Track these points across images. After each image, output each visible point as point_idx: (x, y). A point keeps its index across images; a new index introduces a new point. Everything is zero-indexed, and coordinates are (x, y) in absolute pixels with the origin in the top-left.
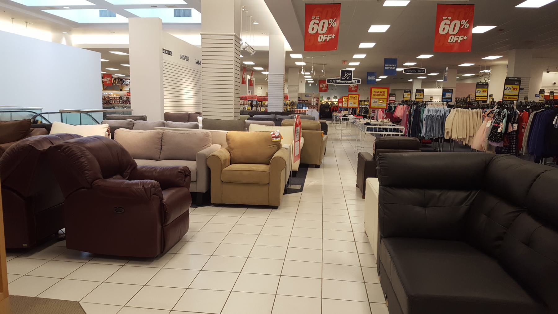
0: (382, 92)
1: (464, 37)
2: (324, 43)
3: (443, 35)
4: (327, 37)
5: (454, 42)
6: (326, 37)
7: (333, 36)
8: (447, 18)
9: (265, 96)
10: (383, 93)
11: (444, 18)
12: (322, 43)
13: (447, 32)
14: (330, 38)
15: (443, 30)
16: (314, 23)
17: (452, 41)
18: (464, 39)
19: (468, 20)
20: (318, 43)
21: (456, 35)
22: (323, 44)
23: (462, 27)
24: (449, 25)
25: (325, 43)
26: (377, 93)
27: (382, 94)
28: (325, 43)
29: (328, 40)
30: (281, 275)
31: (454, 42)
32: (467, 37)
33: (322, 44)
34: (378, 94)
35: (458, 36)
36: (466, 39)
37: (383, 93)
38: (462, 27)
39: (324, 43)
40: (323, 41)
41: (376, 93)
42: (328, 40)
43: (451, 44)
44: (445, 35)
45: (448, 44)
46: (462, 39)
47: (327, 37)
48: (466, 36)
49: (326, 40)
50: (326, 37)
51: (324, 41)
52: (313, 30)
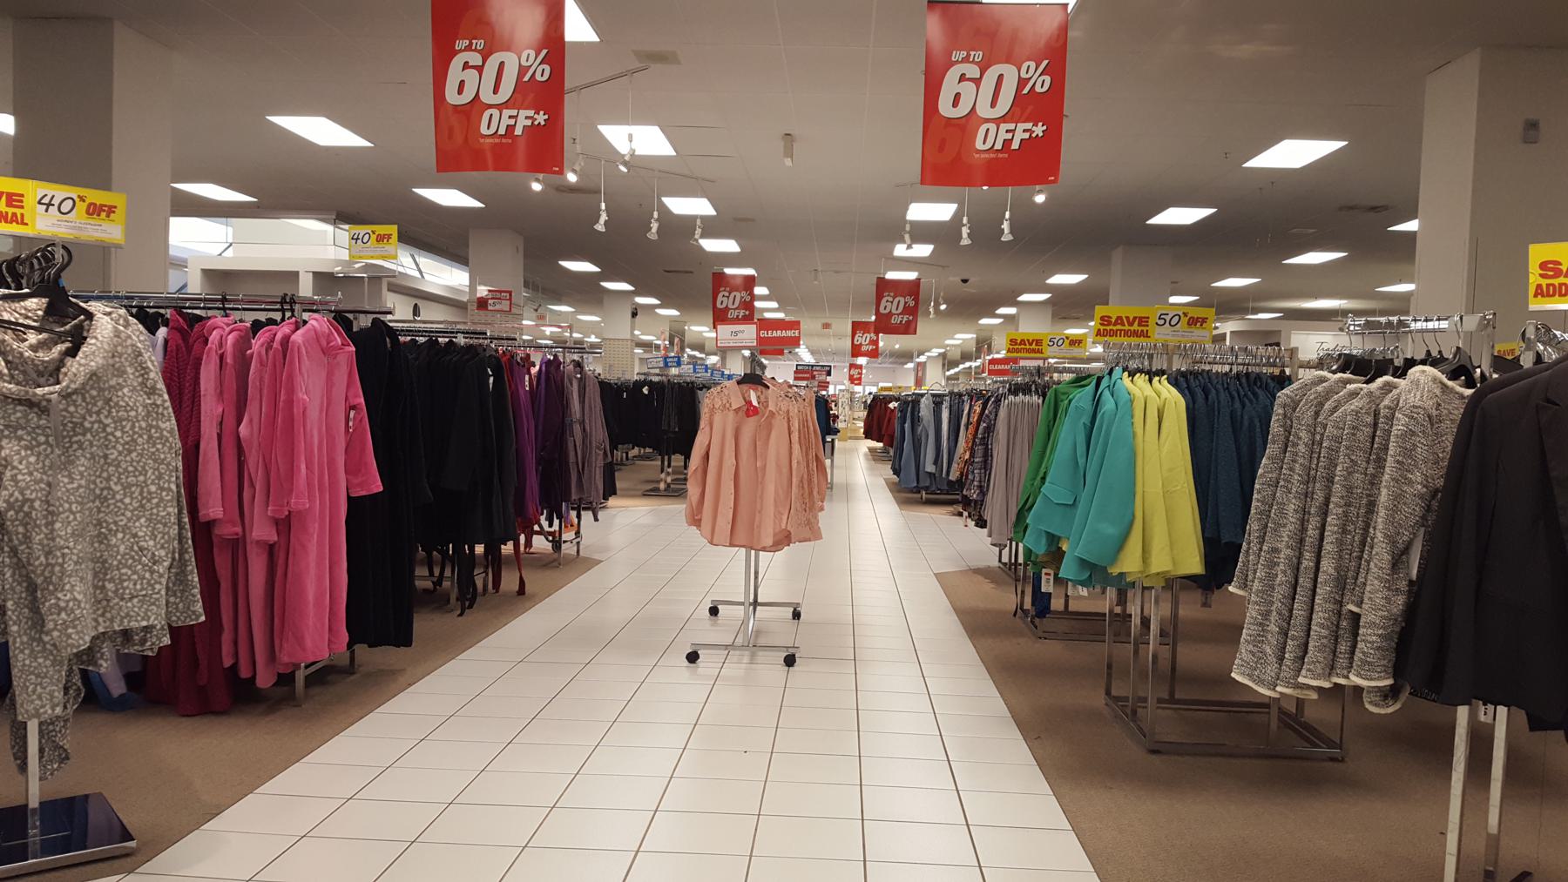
0: (1033, 340)
1: (536, 116)
2: (1000, 155)
3: (953, 122)
4: (1013, 131)
5: (996, 148)
6: (510, 117)
7: (1039, 130)
8: (471, 44)
9: (199, 292)
10: (1036, 345)
11: (461, 44)
12: (992, 156)
13: (474, 95)
14: (1026, 136)
15: (956, 103)
16: (466, 66)
17: (988, 146)
18: (536, 123)
19: (1046, 62)
20: (482, 140)
21: (1003, 119)
22: (997, 159)
23: (1026, 91)
24: (977, 82)
25: (510, 141)
26: (1020, 344)
27: (1033, 346)
28: (1006, 155)
29: (1015, 145)
30: (759, 815)
31: (996, 148)
32: (546, 117)
33: (496, 144)
34: (1023, 346)
35: (1012, 126)
36: (543, 123)
37: (1036, 345)
38: (1026, 91)
39: (1000, 155)
40: (502, 131)
41: (1016, 344)
42: (1015, 145)
43: (987, 156)
44: (469, 106)
45: (978, 155)
46: (529, 123)
47: (1013, 131)
48: (1040, 124)
49: (1007, 143)
50: (510, 117)
51: (1000, 148)
52: (460, 91)
